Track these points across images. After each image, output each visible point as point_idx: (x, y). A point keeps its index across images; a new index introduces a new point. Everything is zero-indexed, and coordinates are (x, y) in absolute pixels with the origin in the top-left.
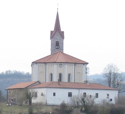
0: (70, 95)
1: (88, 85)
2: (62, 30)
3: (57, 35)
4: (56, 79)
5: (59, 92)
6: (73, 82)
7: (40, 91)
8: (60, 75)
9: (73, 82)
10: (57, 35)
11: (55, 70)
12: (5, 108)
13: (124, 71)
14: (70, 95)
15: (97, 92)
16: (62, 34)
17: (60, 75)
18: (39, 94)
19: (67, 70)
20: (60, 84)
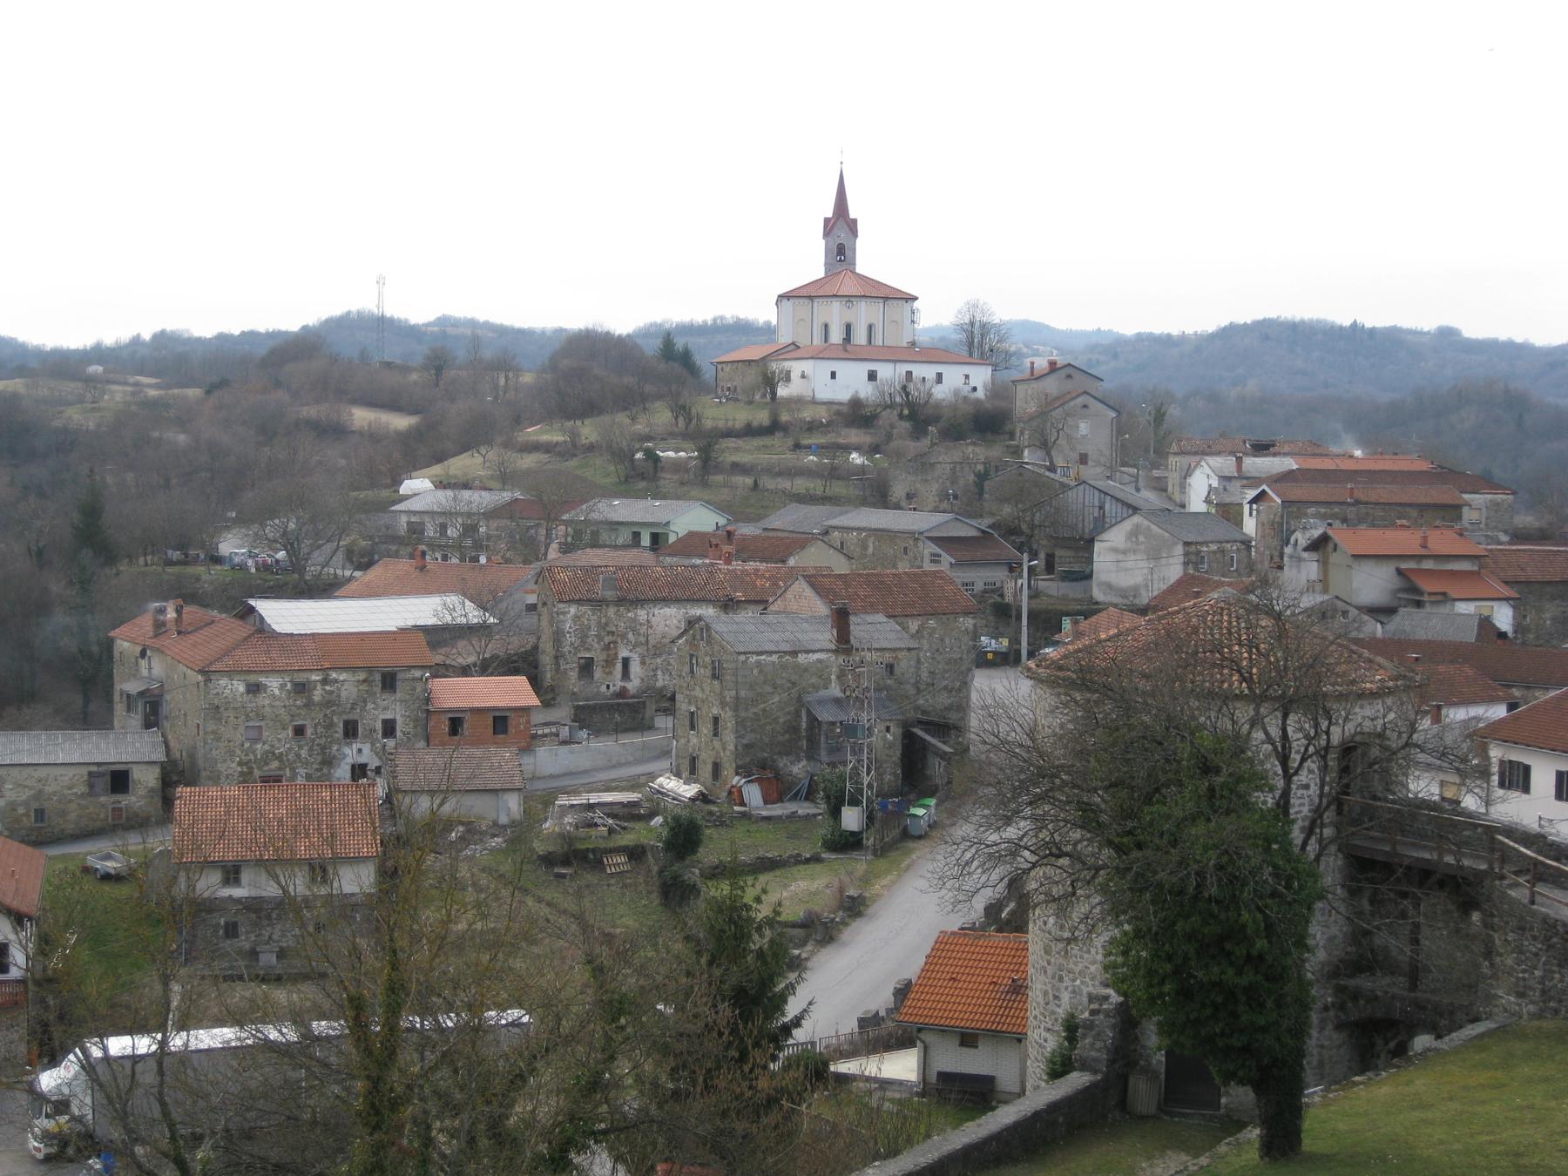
0: (872, 376)
3: (840, 229)
4: (836, 336)
5: (842, 368)
7: (796, 368)
8: (848, 327)
10: (840, 229)
11: (834, 314)
14: (872, 376)
16: (852, 226)
17: (848, 327)
19: (864, 315)
20: (847, 349)
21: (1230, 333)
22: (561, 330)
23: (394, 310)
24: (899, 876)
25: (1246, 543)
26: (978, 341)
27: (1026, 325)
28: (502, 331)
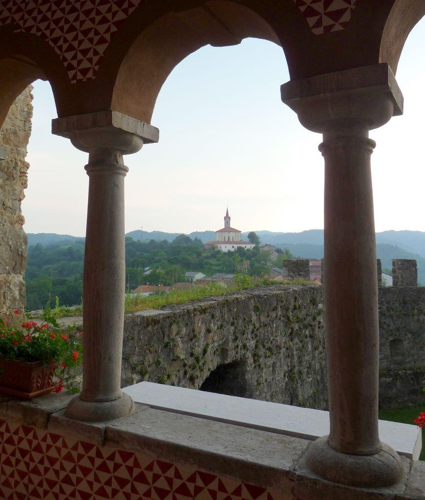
0: (233, 247)
1: (241, 242)
2: (27, 159)
3: (227, 218)
4: (227, 240)
5: (228, 246)
6: (232, 240)
7: (219, 245)
8: (229, 237)
9: (232, 240)
10: (227, 218)
11: (226, 235)
12: (396, 210)
13: (424, 231)
14: (233, 247)
15: (245, 245)
16: (229, 218)
17: (229, 237)
18: (218, 247)
19: (232, 235)
20: (228, 242)
21: (305, 232)
22: (177, 234)
23: (144, 230)
24: (213, 244)
25: (150, 295)
26: (252, 237)
27: (262, 232)
28: (124, 199)
